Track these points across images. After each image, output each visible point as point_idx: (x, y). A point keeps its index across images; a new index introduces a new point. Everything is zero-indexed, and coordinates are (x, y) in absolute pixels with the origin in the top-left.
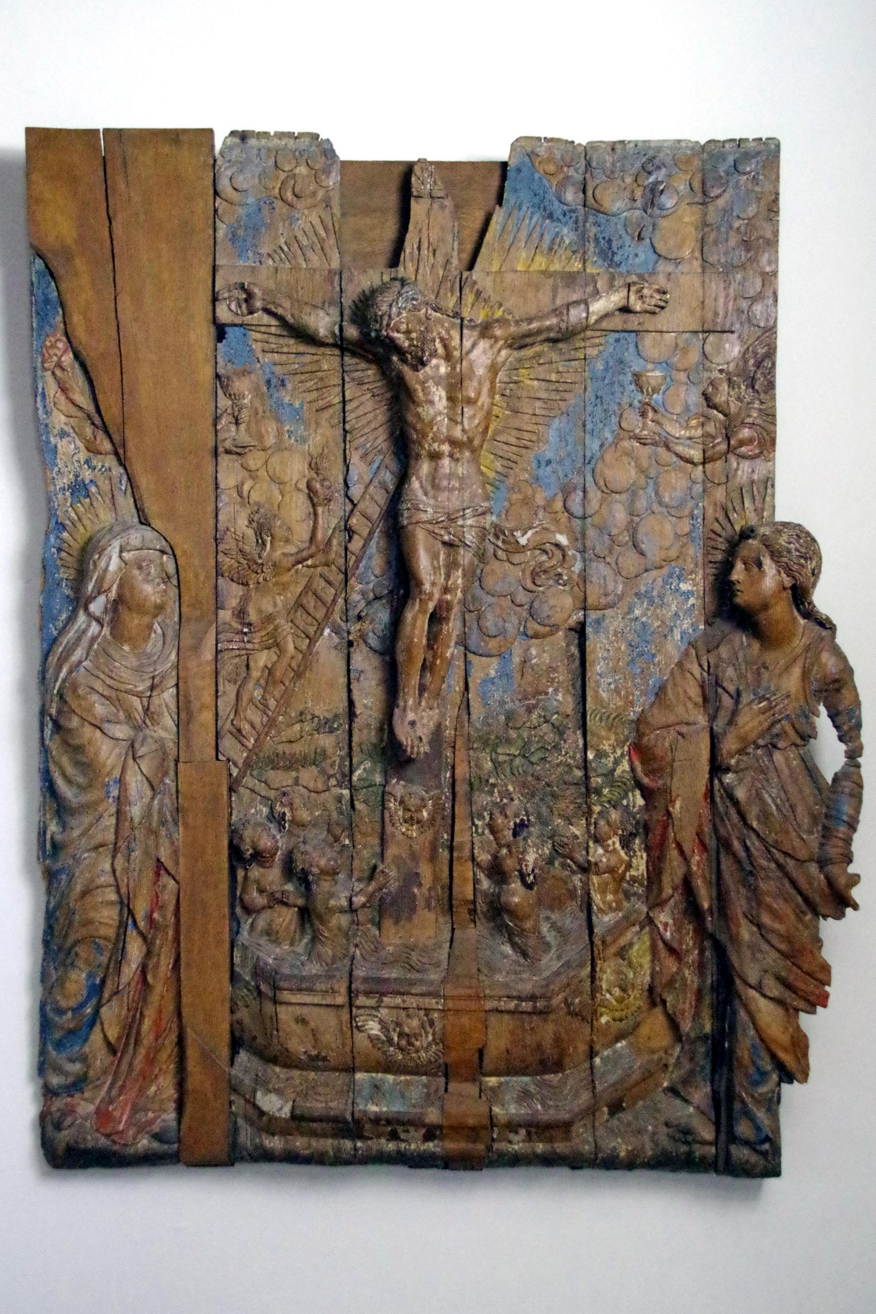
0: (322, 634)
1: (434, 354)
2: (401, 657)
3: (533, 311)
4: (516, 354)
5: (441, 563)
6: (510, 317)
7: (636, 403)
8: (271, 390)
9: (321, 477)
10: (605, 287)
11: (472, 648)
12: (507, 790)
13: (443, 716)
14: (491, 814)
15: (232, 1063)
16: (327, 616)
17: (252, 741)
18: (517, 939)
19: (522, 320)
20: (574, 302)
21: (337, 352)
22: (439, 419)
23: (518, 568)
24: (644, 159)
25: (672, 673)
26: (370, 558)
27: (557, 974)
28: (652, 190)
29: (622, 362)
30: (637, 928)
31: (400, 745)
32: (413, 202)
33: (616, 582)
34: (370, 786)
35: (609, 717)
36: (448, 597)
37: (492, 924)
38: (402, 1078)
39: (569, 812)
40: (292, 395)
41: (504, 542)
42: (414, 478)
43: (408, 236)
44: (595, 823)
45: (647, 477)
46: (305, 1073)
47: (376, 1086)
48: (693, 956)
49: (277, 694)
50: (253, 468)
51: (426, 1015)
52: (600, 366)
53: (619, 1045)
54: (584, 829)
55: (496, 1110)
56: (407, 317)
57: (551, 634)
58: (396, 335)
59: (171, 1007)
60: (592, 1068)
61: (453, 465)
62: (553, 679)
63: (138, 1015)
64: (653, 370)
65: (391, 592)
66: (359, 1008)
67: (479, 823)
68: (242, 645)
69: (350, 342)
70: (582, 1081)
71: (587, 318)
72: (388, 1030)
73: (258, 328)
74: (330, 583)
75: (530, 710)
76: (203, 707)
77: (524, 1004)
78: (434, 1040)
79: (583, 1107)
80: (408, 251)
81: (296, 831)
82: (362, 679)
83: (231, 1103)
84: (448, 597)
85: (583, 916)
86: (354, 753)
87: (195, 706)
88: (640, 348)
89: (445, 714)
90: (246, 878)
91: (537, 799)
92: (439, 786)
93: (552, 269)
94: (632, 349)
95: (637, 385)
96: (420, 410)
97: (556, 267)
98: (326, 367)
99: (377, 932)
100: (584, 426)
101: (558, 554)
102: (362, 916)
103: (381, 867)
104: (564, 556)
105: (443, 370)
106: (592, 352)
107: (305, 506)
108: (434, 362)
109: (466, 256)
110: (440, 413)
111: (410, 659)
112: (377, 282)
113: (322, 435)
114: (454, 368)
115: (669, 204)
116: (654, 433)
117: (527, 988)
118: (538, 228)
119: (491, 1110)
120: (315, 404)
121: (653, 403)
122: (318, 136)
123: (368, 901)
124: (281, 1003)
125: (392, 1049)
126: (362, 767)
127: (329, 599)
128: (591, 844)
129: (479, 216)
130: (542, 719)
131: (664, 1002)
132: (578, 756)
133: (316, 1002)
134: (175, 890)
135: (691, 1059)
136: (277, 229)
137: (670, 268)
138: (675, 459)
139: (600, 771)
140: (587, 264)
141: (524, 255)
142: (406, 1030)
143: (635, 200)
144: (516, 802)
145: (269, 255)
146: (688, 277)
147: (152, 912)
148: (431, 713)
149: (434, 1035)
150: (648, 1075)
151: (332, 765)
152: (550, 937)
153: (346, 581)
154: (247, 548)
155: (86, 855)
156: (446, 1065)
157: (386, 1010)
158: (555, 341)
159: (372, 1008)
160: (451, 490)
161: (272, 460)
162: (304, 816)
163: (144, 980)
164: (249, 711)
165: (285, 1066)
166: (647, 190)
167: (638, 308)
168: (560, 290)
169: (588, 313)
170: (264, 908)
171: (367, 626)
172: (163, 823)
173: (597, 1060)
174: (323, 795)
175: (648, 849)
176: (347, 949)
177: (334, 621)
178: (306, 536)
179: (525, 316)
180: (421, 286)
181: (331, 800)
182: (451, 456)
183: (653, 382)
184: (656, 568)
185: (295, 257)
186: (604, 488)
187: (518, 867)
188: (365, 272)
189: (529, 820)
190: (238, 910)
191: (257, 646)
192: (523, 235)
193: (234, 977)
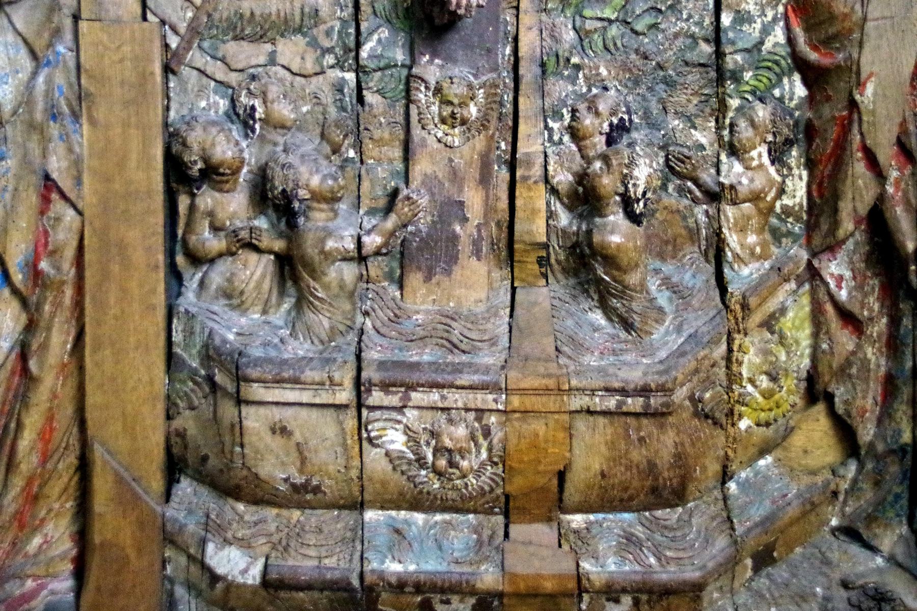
12: (598, 74)
14: (574, 111)
15: (167, 496)
18: (614, 302)
27: (680, 353)
30: (793, 285)
34: (388, 67)
37: (572, 281)
38: (438, 517)
39: (691, 109)
44: (732, 125)
46: (285, 512)
47: (397, 531)
48: (879, 327)
51: (479, 419)
53: (762, 462)
54: (713, 137)
55: (587, 566)
59: (68, 411)
60: (725, 499)
63: (13, 425)
66: (372, 408)
67: (555, 125)
70: (713, 518)
72: (418, 443)
77: (630, 400)
78: (490, 458)
79: (720, 559)
83: (164, 562)
85: (711, 269)
86: (363, 16)
90: (192, 208)
91: (642, 90)
92: (495, 69)
99: (398, 294)
102: (375, 268)
103: (405, 192)
117: (635, 376)
119: (578, 565)
123: (386, 244)
125: (423, 472)
126: (375, 37)
128: (723, 157)
131: (829, 398)
132: (707, 21)
134: (77, 224)
135: (877, 484)
139: (740, 45)
142: (448, 443)
144: (612, 92)
147: (36, 259)
149: (490, 450)
150: (810, 507)
151: (328, 33)
152: (663, 298)
156: (507, 497)
157: (416, 412)
159: (394, 408)
162: (286, 112)
163: (25, 371)
165: (257, 501)
170: (221, 255)
172: (54, 115)
173: (732, 486)
174: (314, 80)
175: (810, 165)
176: (352, 319)
181: (326, 89)
187: (621, 190)
189: (631, 120)
190: (180, 259)
193: (171, 360)
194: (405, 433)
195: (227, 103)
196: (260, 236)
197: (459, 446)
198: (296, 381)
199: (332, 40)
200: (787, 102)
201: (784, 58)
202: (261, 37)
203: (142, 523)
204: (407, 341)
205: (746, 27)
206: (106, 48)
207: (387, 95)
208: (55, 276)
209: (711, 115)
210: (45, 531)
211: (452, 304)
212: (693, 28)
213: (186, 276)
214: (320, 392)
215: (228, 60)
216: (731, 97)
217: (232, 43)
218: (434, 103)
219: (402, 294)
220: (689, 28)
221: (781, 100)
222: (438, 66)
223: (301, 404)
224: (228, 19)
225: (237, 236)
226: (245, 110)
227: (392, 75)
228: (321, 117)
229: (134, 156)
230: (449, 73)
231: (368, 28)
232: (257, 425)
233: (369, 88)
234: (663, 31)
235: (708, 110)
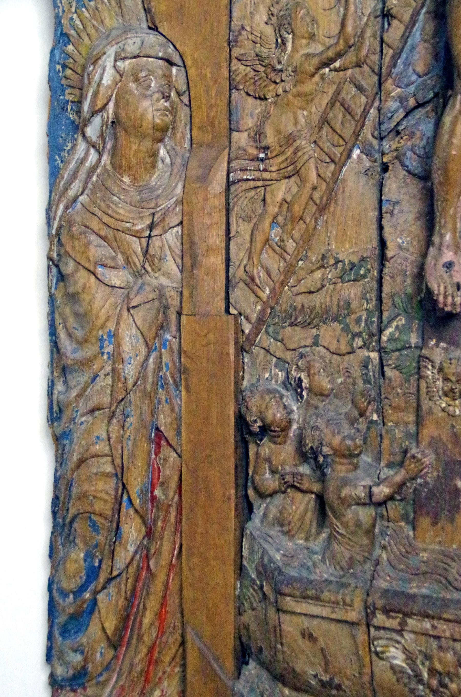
16: (356, 135)
17: (268, 291)
26: (413, 49)
34: (404, 348)
65: (436, 95)
66: (378, 628)
68: (257, 174)
74: (360, 88)
76: (209, 250)
81: (315, 401)
82: (396, 212)
86: (384, 307)
87: (201, 248)
99: (411, 533)
103: (414, 451)
124: (285, 612)
126: (394, 324)
127: (359, 111)
133: (324, 614)
142: (438, 666)
151: (358, 321)
153: (380, 84)
154: (264, 52)
155: (84, 419)
157: (412, 636)
174: (346, 358)
177: (365, 138)
178: (335, 30)
190: (250, 492)
191: (274, 174)
194: (404, 652)
195: (284, 374)
196: (301, 480)
197: (447, 670)
198: (318, 599)
199: (360, 326)
202: (309, 324)
203: (218, 692)
204: (412, 574)
206: (199, 335)
207: (403, 371)
208: (163, 500)
210: (162, 687)
211: (454, 546)
213: (255, 506)
214: (336, 609)
215: (286, 342)
217: (289, 328)
218: (438, 379)
219: (414, 534)
222: (443, 348)
223: (322, 618)
225: (284, 479)
227: (407, 355)
229: (215, 415)
231: (388, 318)
232: (291, 629)
233: (388, 365)
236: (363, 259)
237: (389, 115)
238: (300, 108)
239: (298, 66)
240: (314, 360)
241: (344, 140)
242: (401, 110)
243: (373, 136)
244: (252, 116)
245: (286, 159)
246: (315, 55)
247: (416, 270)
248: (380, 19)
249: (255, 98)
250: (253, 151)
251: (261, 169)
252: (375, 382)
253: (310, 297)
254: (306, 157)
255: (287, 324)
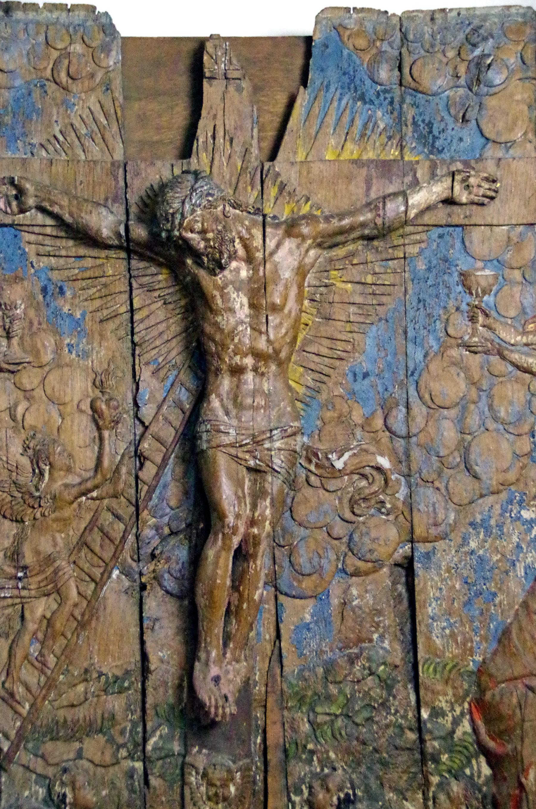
0: (109, 577)
1: (233, 256)
2: (201, 601)
3: (345, 205)
4: (327, 254)
5: (246, 491)
6: (318, 213)
7: (464, 307)
8: (48, 298)
9: (107, 397)
10: (427, 178)
11: (284, 588)
12: (328, 757)
13: (251, 669)
14: (310, 788)
16: (115, 556)
17: (27, 706)
19: (332, 216)
20: (389, 195)
21: (123, 255)
22: (240, 328)
23: (333, 496)
24: (468, 30)
25: (517, 614)
26: (165, 486)
28: (478, 64)
29: (446, 261)
31: (201, 705)
32: (205, 83)
33: (447, 509)
34: (167, 756)
35: (444, 667)
36: (255, 531)
39: (402, 784)
40: (72, 304)
41: (317, 466)
42: (213, 396)
43: (201, 124)
44: (434, 799)
45: (480, 390)
49: (57, 649)
50: (28, 387)
52: (421, 266)
56: (202, 216)
57: (375, 570)
58: (189, 235)
61: (257, 380)
62: (378, 624)
64: (483, 269)
65: (189, 526)
67: (296, 799)
68: (16, 592)
69: (138, 244)
71: (406, 212)
73: (31, 229)
74: (118, 517)
75: (352, 661)
80: (201, 140)
82: (157, 627)
84: (255, 531)
86: (148, 718)
88: (467, 244)
89: (253, 668)
91: (363, 769)
93: (365, 157)
94: (458, 245)
95: (464, 285)
96: (219, 319)
97: (371, 155)
98: (110, 272)
100: (405, 333)
101: (379, 479)
104: (386, 481)
105: (244, 274)
106: (413, 250)
107: (90, 431)
108: (234, 264)
109: (267, 145)
110: (242, 322)
111: (212, 605)
112: (167, 175)
113: (108, 349)
114: (256, 270)
115: (498, 80)
116: (486, 340)
118: (348, 112)
120: (99, 314)
121: (483, 305)
122: (94, 8)
126: (158, 733)
127: (118, 536)
129: (282, 99)
130: (367, 672)
132: (410, 715)
136: (51, 115)
137: (500, 154)
138: (511, 368)
139: (437, 733)
140: (406, 150)
141: (333, 142)
143: (458, 77)
144: (340, 772)
145: (42, 146)
146: (521, 163)
148: (237, 666)
151: (122, 732)
153: (138, 515)
154: (22, 480)
158: (370, 238)
160: (255, 408)
161: (51, 377)
162: (89, 797)
164: (24, 671)
166: (472, 64)
167: (464, 199)
168: (374, 181)
169: (407, 206)
171: (161, 566)
174: (111, 769)
178: (91, 464)
179: (336, 211)
180: (216, 179)
182: (255, 370)
183: (483, 283)
184: (493, 493)
185: (71, 147)
186: (430, 403)
188: (153, 164)
189: (355, 794)
191: (33, 593)
192: (331, 119)
200: (476, 779)
201: (472, 745)
205: (440, 720)
209: (419, 789)
212: (400, 720)
216: (432, 775)
217: (50, 743)
220: (397, 720)
221: (471, 777)
222: (205, 755)
224: (47, 725)
226: (59, 796)
228: (116, 799)
230: (214, 761)
233: (152, 774)
234: (377, 723)
235: (415, 784)
236: (127, 673)
237: (147, 541)
238: (58, 531)
239: (57, 495)
240: (78, 774)
241: (104, 562)
242: (157, 537)
243: (133, 560)
244: (8, 537)
245: (46, 578)
246: (74, 486)
247: (177, 682)
248: (133, 459)
249: (12, 520)
250: (12, 571)
251: (20, 587)
252: (140, 791)
253: (73, 710)
254: (66, 577)
255: (47, 739)
